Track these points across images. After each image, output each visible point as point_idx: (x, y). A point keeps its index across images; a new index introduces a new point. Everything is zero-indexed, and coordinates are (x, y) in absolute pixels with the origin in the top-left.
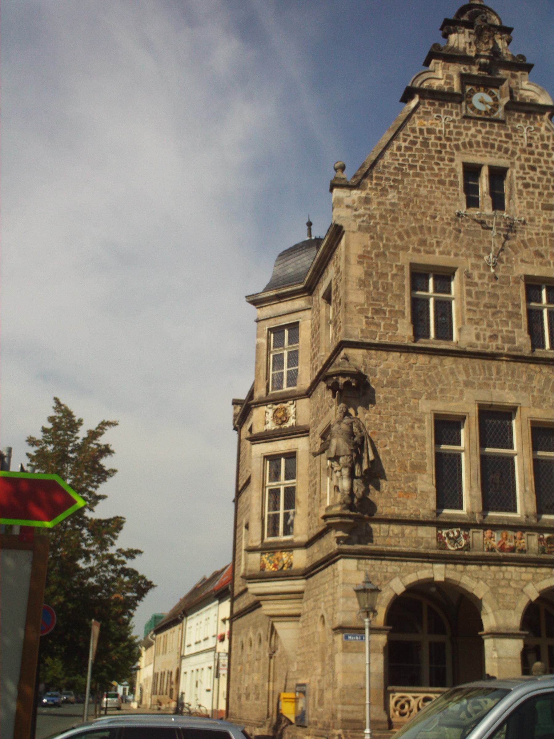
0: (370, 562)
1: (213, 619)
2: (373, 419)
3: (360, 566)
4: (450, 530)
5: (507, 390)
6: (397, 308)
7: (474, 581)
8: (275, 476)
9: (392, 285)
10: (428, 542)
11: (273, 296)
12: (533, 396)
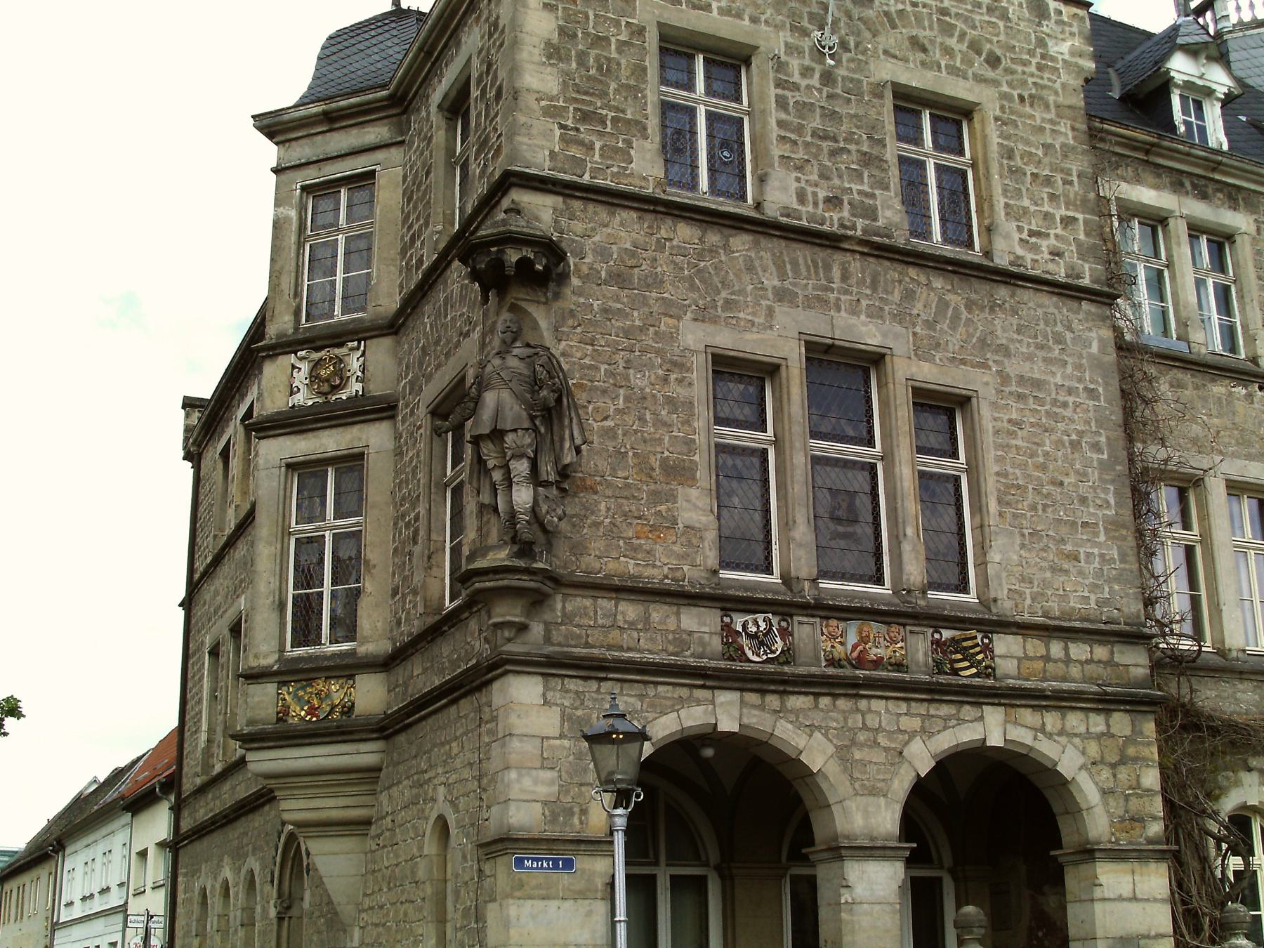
0: (572, 685)
1: (118, 853)
2: (579, 355)
3: (550, 695)
4: (749, 617)
5: (863, 317)
6: (629, 116)
7: (806, 735)
8: (311, 510)
9: (619, 64)
10: (702, 643)
11: (316, 115)
12: (915, 334)
